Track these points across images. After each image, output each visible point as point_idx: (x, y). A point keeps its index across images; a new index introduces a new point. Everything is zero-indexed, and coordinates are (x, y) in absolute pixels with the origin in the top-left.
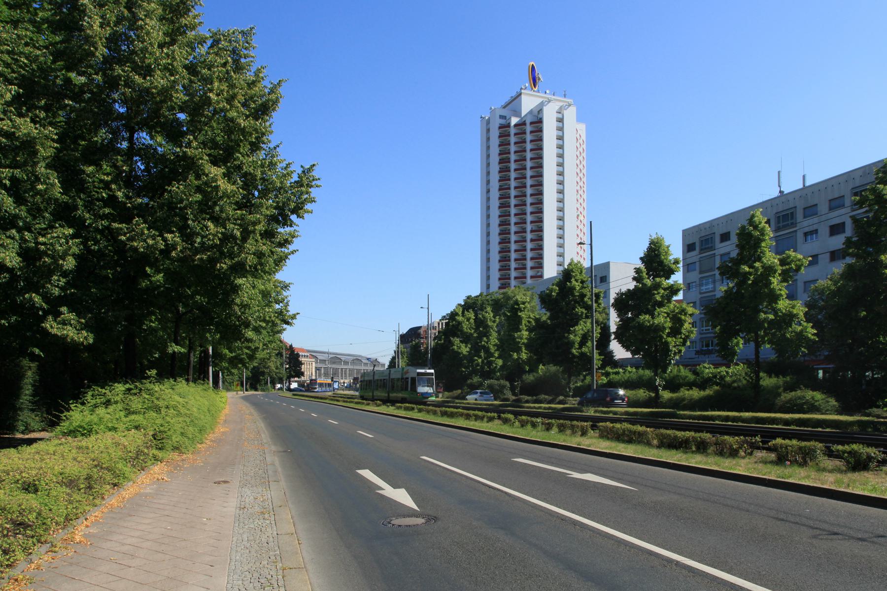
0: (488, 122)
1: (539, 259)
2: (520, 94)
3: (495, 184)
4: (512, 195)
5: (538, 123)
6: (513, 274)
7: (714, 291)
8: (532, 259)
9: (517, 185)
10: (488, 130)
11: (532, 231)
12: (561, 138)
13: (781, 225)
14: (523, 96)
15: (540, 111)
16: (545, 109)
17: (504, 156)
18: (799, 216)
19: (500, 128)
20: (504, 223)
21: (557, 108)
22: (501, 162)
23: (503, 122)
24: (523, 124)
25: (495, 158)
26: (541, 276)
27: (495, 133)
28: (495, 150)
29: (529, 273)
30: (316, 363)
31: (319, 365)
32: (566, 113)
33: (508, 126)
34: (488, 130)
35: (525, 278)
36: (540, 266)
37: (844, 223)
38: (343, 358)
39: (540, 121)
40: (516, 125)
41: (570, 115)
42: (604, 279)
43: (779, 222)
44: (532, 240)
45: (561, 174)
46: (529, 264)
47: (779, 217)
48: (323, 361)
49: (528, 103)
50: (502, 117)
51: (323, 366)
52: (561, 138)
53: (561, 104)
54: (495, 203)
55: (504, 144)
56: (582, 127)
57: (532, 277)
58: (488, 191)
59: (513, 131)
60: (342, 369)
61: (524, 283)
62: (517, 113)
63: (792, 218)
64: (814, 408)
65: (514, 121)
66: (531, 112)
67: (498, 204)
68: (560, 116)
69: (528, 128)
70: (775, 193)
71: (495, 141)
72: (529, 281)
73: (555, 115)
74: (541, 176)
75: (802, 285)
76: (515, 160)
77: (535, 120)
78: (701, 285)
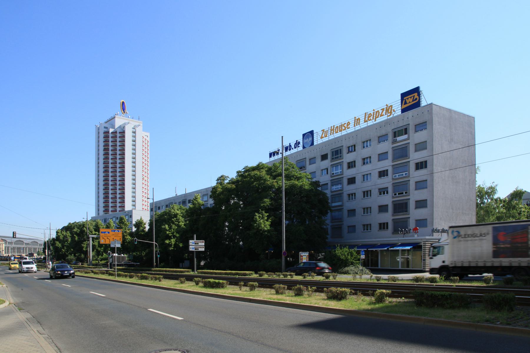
0: (99, 129)
2: (115, 117)
3: (102, 161)
7: (343, 174)
8: (119, 198)
10: (99, 133)
11: (119, 185)
13: (334, 157)
14: (116, 119)
15: (124, 127)
16: (126, 127)
17: (106, 147)
18: (345, 151)
19: (104, 133)
20: (106, 180)
21: (133, 126)
22: (105, 150)
23: (106, 130)
24: (116, 132)
25: (102, 148)
27: (102, 135)
28: (102, 144)
30: (6, 243)
31: (8, 245)
32: (137, 129)
33: (108, 132)
34: (99, 133)
38: (25, 241)
40: (112, 133)
41: (139, 130)
42: (131, 216)
43: (333, 155)
44: (119, 189)
46: (118, 200)
47: (333, 152)
48: (11, 243)
49: (119, 122)
50: (105, 128)
51: (10, 246)
54: (102, 170)
55: (106, 141)
57: (112, 211)
58: (98, 163)
59: (110, 135)
60: (23, 248)
62: (113, 127)
63: (341, 153)
64: (250, 275)
65: (111, 130)
66: (120, 127)
68: (134, 130)
69: (118, 135)
70: (175, 195)
71: (102, 139)
73: (132, 130)
76: (112, 148)
77: (122, 131)
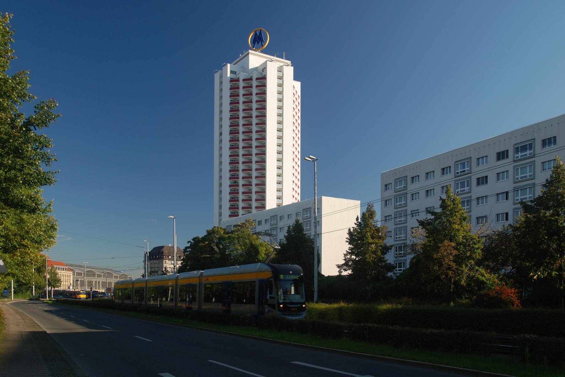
1: (262, 193)
4: (241, 139)
5: (262, 79)
6: (241, 204)
9: (245, 123)
12: (280, 93)
23: (234, 76)
26: (263, 207)
29: (254, 204)
35: (251, 208)
36: (263, 199)
37: (507, 151)
39: (264, 78)
44: (256, 200)
45: (280, 100)
52: (280, 93)
53: (282, 64)
56: (298, 85)
61: (251, 212)
67: (228, 206)
72: (254, 211)
74: (264, 169)
75: (475, 219)
77: (260, 76)
78: (396, 185)
